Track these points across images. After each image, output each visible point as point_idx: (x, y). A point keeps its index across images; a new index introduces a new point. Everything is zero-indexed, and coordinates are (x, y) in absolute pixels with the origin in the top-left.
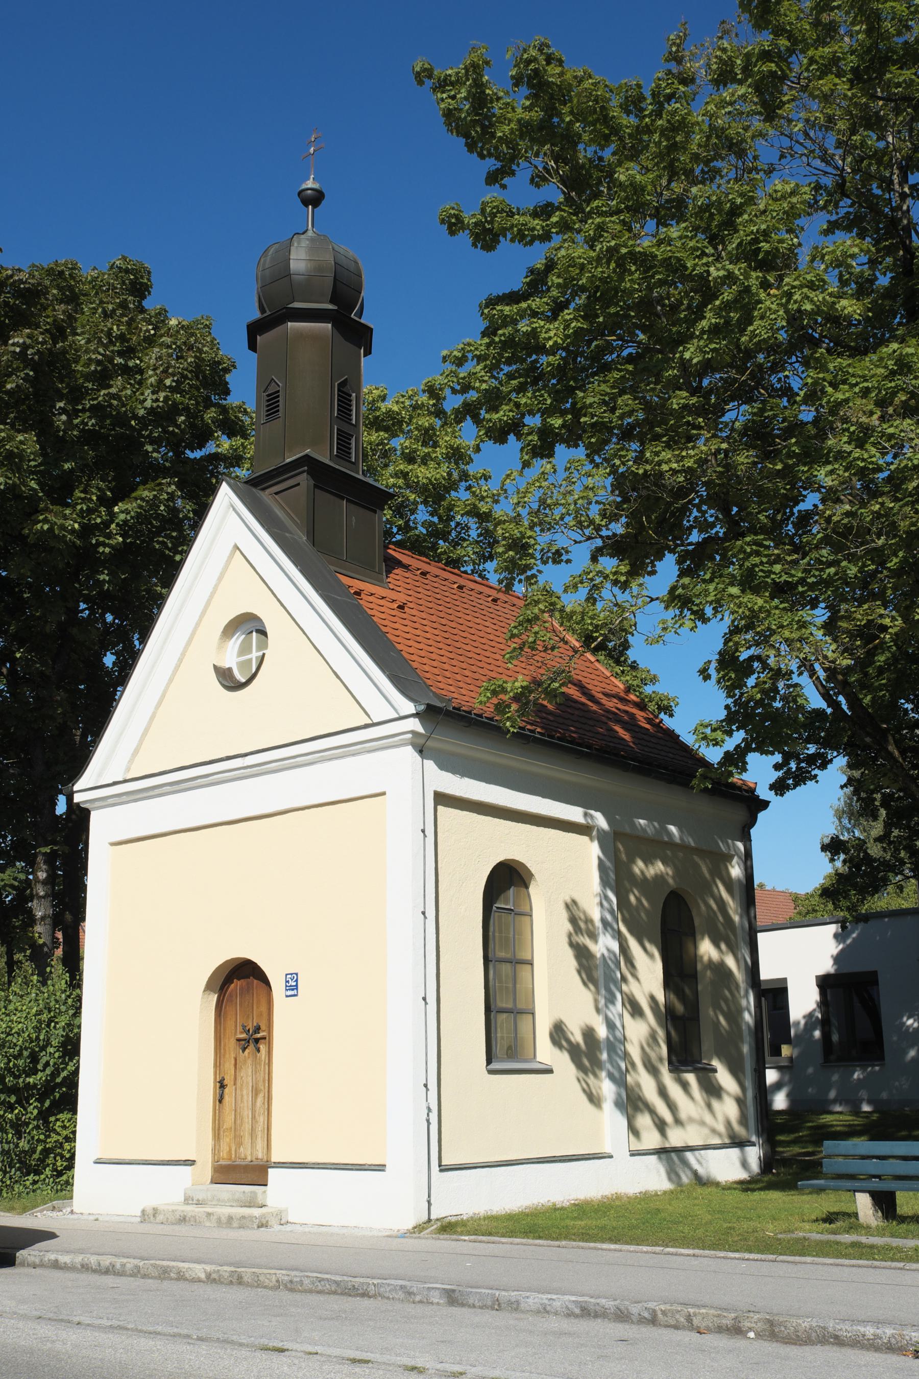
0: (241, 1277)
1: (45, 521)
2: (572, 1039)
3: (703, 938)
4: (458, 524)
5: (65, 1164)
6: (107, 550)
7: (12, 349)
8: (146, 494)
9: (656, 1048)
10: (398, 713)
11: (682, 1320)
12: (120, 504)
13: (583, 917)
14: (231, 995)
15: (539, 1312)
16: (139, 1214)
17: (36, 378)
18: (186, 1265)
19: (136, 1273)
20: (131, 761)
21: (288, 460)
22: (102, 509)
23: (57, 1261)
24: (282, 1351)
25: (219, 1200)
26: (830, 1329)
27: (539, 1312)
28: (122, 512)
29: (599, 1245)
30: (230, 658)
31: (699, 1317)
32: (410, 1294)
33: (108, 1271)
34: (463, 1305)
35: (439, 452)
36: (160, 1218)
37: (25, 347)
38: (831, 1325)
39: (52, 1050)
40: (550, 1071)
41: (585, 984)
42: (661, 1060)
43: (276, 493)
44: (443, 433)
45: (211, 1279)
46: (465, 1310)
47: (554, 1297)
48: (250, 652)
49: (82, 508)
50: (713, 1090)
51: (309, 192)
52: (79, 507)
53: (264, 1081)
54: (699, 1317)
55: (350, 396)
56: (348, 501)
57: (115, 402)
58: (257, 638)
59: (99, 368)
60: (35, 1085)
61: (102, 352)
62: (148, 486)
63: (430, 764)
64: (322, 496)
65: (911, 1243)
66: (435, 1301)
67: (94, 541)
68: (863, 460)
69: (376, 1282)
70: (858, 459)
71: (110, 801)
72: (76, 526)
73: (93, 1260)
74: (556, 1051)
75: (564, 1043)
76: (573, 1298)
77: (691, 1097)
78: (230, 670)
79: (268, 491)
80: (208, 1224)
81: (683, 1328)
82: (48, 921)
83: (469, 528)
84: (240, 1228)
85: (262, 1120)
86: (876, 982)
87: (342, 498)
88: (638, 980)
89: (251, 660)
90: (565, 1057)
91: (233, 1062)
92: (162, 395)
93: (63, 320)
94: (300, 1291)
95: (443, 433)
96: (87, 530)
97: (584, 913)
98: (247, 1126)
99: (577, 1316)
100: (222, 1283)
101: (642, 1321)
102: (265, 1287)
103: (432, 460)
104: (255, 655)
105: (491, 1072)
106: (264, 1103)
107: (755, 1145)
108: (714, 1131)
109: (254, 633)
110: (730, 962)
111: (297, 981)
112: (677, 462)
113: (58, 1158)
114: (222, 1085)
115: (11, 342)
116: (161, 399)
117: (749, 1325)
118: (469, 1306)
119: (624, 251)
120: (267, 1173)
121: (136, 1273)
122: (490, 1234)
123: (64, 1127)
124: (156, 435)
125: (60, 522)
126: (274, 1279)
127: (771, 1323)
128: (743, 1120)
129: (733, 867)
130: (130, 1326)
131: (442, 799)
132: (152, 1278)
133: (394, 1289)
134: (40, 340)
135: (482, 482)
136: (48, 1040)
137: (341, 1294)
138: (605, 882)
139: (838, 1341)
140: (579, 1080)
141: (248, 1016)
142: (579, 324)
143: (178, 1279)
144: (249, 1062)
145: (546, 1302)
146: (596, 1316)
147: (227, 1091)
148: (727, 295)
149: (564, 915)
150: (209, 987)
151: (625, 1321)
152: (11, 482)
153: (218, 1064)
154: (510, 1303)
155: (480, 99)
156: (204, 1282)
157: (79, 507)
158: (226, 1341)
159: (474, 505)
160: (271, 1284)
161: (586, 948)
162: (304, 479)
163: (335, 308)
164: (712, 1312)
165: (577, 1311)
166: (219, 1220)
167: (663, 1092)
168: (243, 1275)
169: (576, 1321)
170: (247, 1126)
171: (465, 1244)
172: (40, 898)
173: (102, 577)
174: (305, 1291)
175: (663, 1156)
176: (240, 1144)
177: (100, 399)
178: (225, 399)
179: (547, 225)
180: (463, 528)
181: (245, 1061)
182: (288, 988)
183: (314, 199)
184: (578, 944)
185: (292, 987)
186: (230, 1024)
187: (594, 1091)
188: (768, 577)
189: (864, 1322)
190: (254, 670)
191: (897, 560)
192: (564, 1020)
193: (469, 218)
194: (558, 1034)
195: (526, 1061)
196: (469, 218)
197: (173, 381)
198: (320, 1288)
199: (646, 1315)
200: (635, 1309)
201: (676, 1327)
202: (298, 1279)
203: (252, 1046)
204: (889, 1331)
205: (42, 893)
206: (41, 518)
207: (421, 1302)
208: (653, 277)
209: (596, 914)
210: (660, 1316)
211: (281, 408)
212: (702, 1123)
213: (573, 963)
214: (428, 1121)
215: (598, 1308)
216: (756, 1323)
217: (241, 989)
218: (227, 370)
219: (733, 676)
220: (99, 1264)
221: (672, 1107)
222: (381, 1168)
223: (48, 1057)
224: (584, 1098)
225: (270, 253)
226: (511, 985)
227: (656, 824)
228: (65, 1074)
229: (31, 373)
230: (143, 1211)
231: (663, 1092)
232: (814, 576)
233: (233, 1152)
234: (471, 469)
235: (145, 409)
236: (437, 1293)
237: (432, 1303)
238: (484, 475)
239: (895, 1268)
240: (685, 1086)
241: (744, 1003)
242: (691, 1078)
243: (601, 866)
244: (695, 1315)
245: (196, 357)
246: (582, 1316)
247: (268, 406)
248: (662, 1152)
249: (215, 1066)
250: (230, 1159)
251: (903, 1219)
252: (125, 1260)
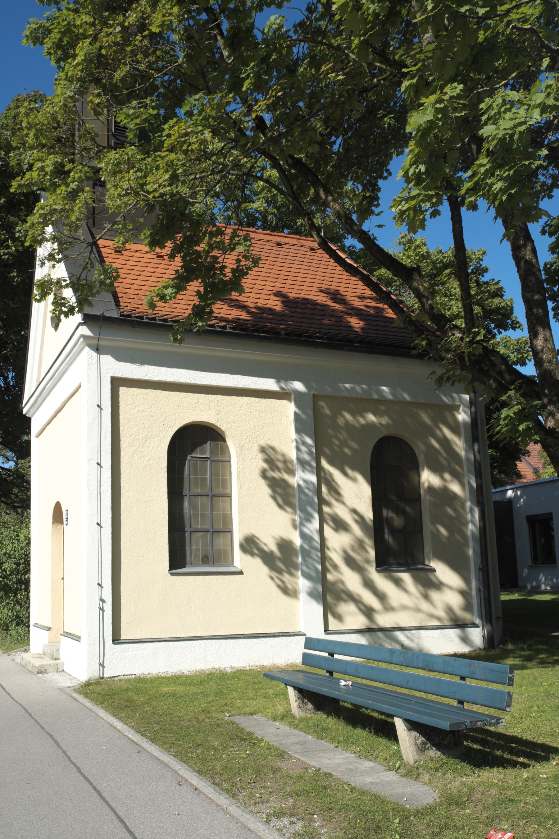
2: (265, 548)
3: (423, 470)
9: (364, 554)
13: (280, 457)
40: (241, 573)
41: (280, 507)
42: (368, 561)
75: (256, 551)
77: (406, 591)
97: (283, 455)
105: (172, 574)
107: (478, 627)
110: (455, 488)
128: (468, 607)
129: (459, 413)
140: (272, 578)
149: (260, 456)
161: (284, 481)
167: (369, 584)
175: (367, 634)
187: (289, 586)
209: (293, 455)
221: (381, 597)
226: (208, 512)
240: (398, 582)
241: (469, 517)
242: (406, 577)
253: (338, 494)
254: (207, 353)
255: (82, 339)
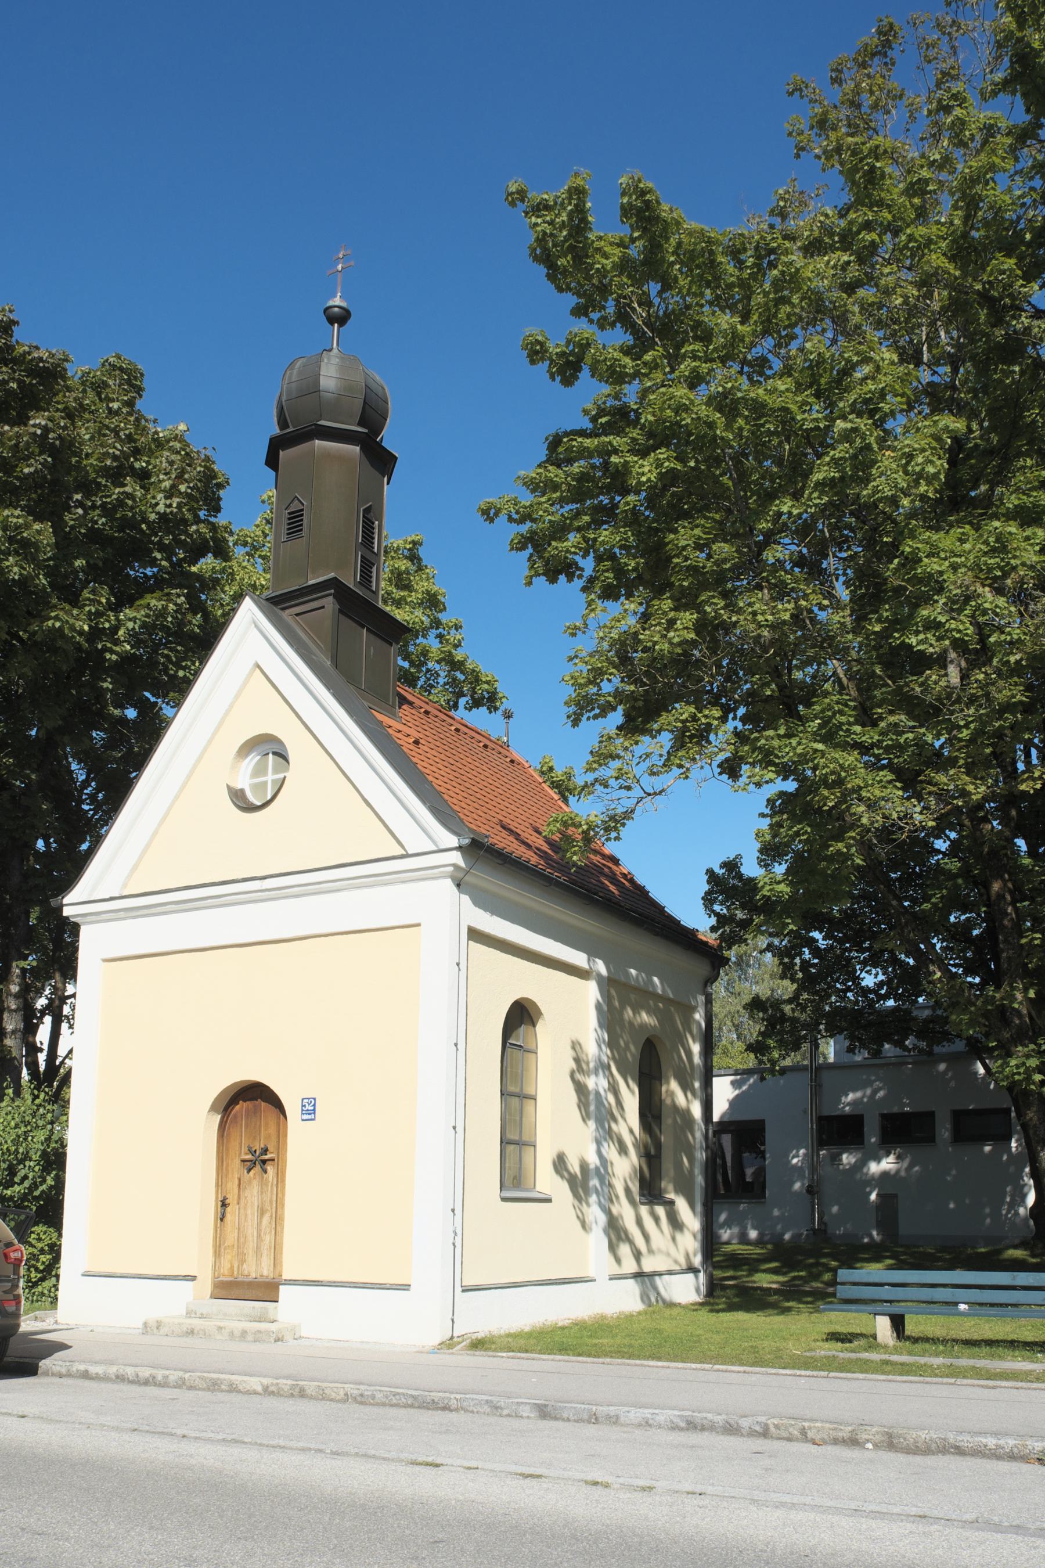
0: (304, 1390)
1: (57, 618)
4: (428, 670)
5: (39, 1275)
6: (114, 657)
7: (32, 430)
8: (153, 602)
10: (436, 845)
11: (796, 1432)
12: (127, 611)
14: (235, 1117)
15: (640, 1425)
16: (141, 1326)
17: (54, 465)
18: (239, 1378)
19: (181, 1384)
20: (129, 877)
21: (311, 582)
22: (111, 614)
23: (87, 1371)
24: (437, 1466)
25: (225, 1314)
26: (951, 1441)
27: (640, 1425)
28: (130, 620)
29: (646, 1362)
30: (243, 781)
31: (814, 1431)
32: (497, 1408)
33: (137, 1381)
34: (556, 1419)
35: (413, 597)
36: (164, 1330)
37: (46, 430)
38: (951, 1437)
39: (32, 1164)
40: (548, 1200)
43: (297, 615)
44: (417, 578)
45: (267, 1391)
46: (559, 1424)
47: (656, 1411)
48: (265, 774)
49: (90, 611)
50: (676, 1224)
51: (336, 309)
52: (87, 609)
53: (271, 1202)
54: (814, 1431)
55: (373, 523)
56: (368, 630)
57: (130, 502)
58: (274, 760)
59: (115, 464)
60: (11, 1198)
61: (119, 447)
62: (155, 595)
63: (466, 899)
64: (346, 623)
65: (1037, 1367)
66: (525, 1414)
67: (100, 646)
68: (959, 631)
69: (458, 1396)
70: (954, 630)
71: (104, 917)
72: (86, 628)
73: (130, 1371)
74: (558, 1178)
75: (566, 1174)
76: (677, 1413)
77: (662, 1231)
78: (242, 791)
79: (288, 611)
80: (219, 1337)
81: (797, 1440)
82: (19, 1035)
83: (438, 675)
84: (255, 1341)
85: (268, 1239)
86: (763, 1130)
87: (363, 626)
88: (625, 1120)
89: (266, 783)
90: (565, 1186)
91: (236, 1182)
92: (175, 501)
93: (75, 408)
94: (371, 1404)
95: (417, 578)
96: (96, 634)
98: (251, 1245)
99: (681, 1429)
100: (282, 1396)
101: (752, 1434)
102: (331, 1400)
103: (406, 603)
104: (270, 777)
105: (504, 1199)
106: (270, 1223)
108: (676, 1262)
109: (271, 755)
111: (314, 1105)
112: (773, 614)
113: (32, 1269)
114: (224, 1204)
115: (32, 422)
116: (175, 505)
117: (867, 1437)
118: (563, 1420)
119: (739, 395)
120: (278, 1289)
121: (181, 1384)
122: (527, 1351)
123: (39, 1240)
124: (167, 542)
125: (71, 621)
126: (342, 1393)
127: (890, 1436)
130: (246, 1440)
131: (475, 935)
132: (200, 1389)
133: (480, 1403)
134: (62, 424)
135: (453, 631)
136: (28, 1153)
137: (419, 1407)
138: (601, 1025)
139: (960, 1451)
141: (255, 1138)
142: (672, 465)
143: (230, 1391)
144: (255, 1183)
145: (649, 1416)
146: (703, 1429)
147: (228, 1209)
148: (841, 451)
149: (570, 1054)
150: (214, 1108)
151: (734, 1434)
152: (25, 573)
153: (220, 1183)
154: (608, 1417)
155: (579, 225)
156: (260, 1394)
157: (87, 609)
158: (365, 1456)
159: (450, 652)
160: (338, 1398)
162: (329, 603)
163: (366, 431)
164: (827, 1425)
165: (683, 1425)
166: (232, 1335)
167: (639, 1222)
168: (306, 1388)
169: (682, 1434)
170: (251, 1245)
171: (504, 1361)
172: (11, 1011)
173: (105, 685)
174: (378, 1404)
175: (639, 1279)
176: (242, 1261)
177: (115, 496)
178: (215, 517)
179: (638, 365)
180: (432, 675)
181: (250, 1182)
182: (304, 1111)
183: (341, 318)
184: (579, 1082)
185: (310, 1110)
186: (234, 1144)
188: (848, 736)
189: (984, 1433)
190: (269, 797)
191: (969, 732)
192: (566, 1153)
193: (553, 349)
194: (560, 1163)
195: (527, 1190)
196: (553, 349)
197: (189, 487)
198: (394, 1401)
199: (758, 1428)
200: (745, 1423)
201: (789, 1439)
202: (370, 1393)
203: (258, 1168)
204: (1011, 1442)
205: (13, 1007)
206: (53, 614)
207: (509, 1415)
208: (763, 425)
210: (772, 1429)
211: (305, 527)
212: (668, 1255)
213: (573, 1097)
214: (454, 1244)
215: (705, 1422)
216: (874, 1435)
217: (247, 1111)
218: (220, 486)
219: (809, 830)
220: (137, 1376)
222: (406, 1287)
223: (30, 1170)
224: (578, 1224)
225: (297, 366)
226: (518, 1118)
227: (643, 975)
228: (44, 1187)
229: (49, 459)
230: (145, 1324)
231: (639, 1222)
232: (891, 739)
233: (236, 1269)
234: (443, 617)
235: (158, 513)
236: (527, 1408)
237: (521, 1417)
238: (456, 625)
239: (947, 1384)
240: (657, 1219)
243: (598, 1007)
244: (810, 1428)
245: (205, 467)
246: (687, 1429)
247: (289, 524)
248: (639, 1275)
249: (217, 1185)
250: (232, 1275)
251: (916, 1340)
252: (167, 1372)
253: (623, 1109)
254: (557, 915)
255: (451, 869)
